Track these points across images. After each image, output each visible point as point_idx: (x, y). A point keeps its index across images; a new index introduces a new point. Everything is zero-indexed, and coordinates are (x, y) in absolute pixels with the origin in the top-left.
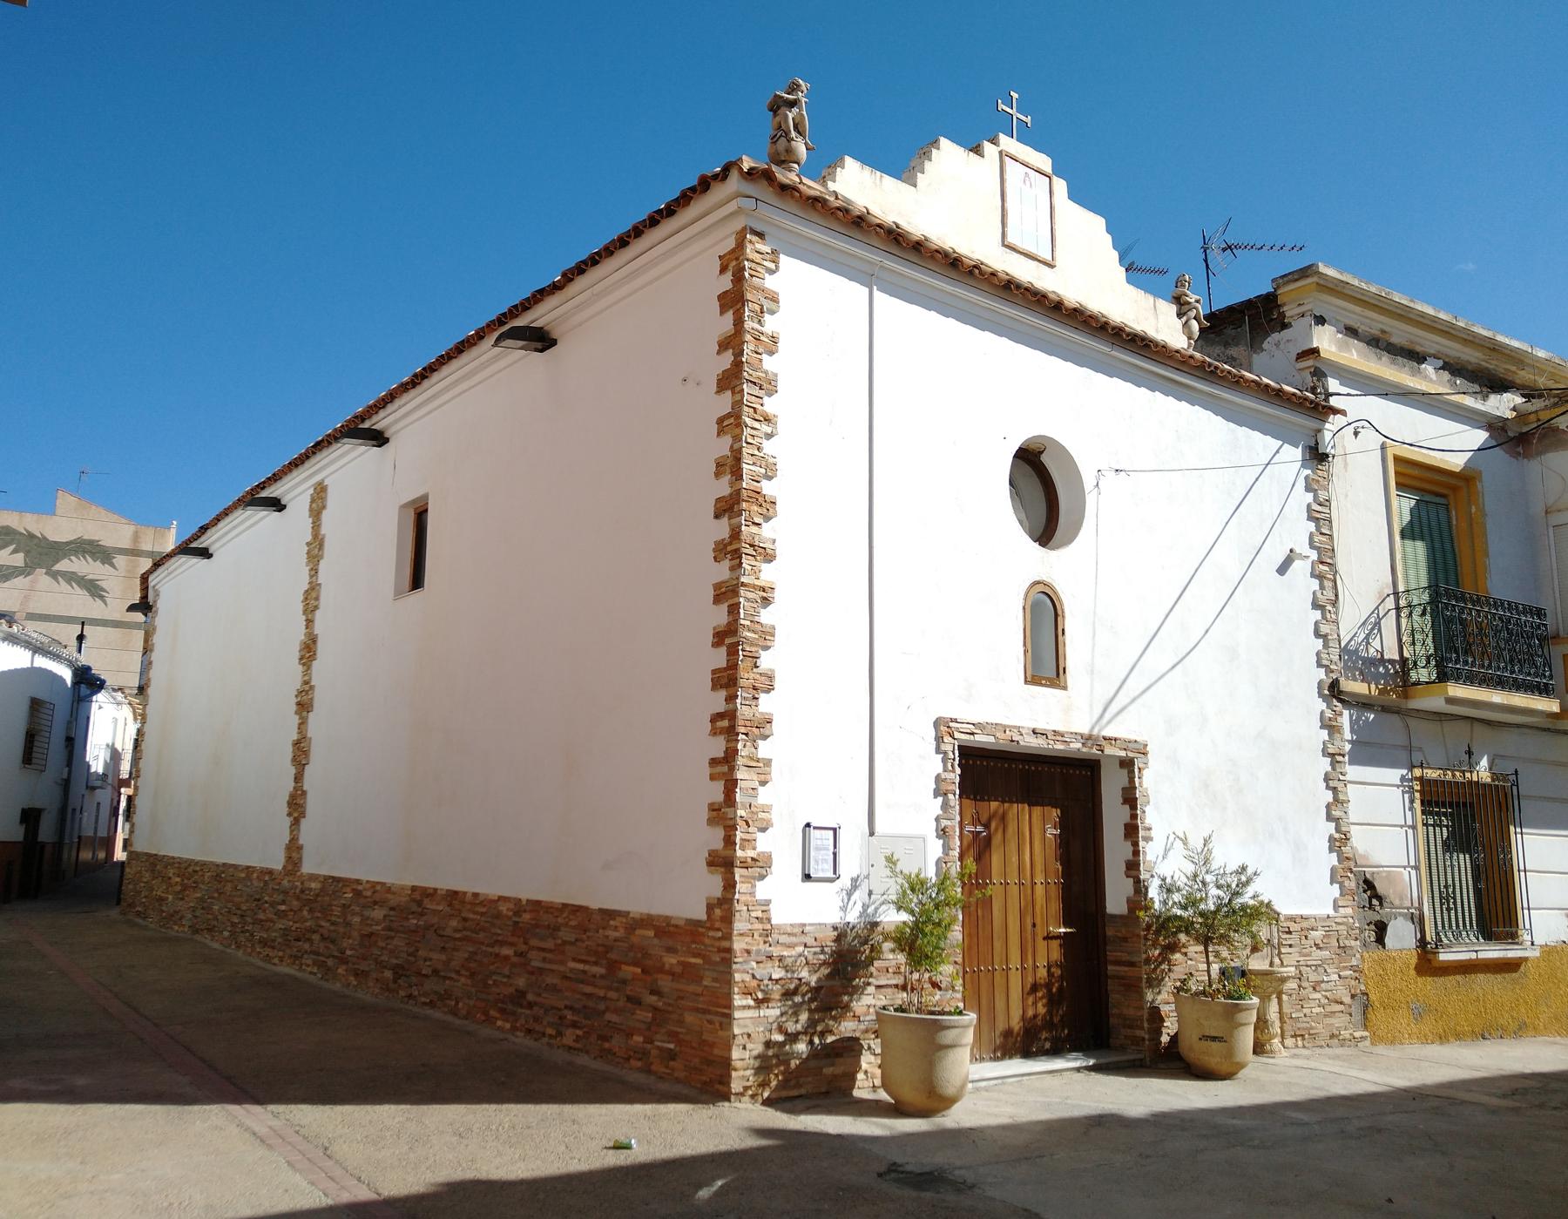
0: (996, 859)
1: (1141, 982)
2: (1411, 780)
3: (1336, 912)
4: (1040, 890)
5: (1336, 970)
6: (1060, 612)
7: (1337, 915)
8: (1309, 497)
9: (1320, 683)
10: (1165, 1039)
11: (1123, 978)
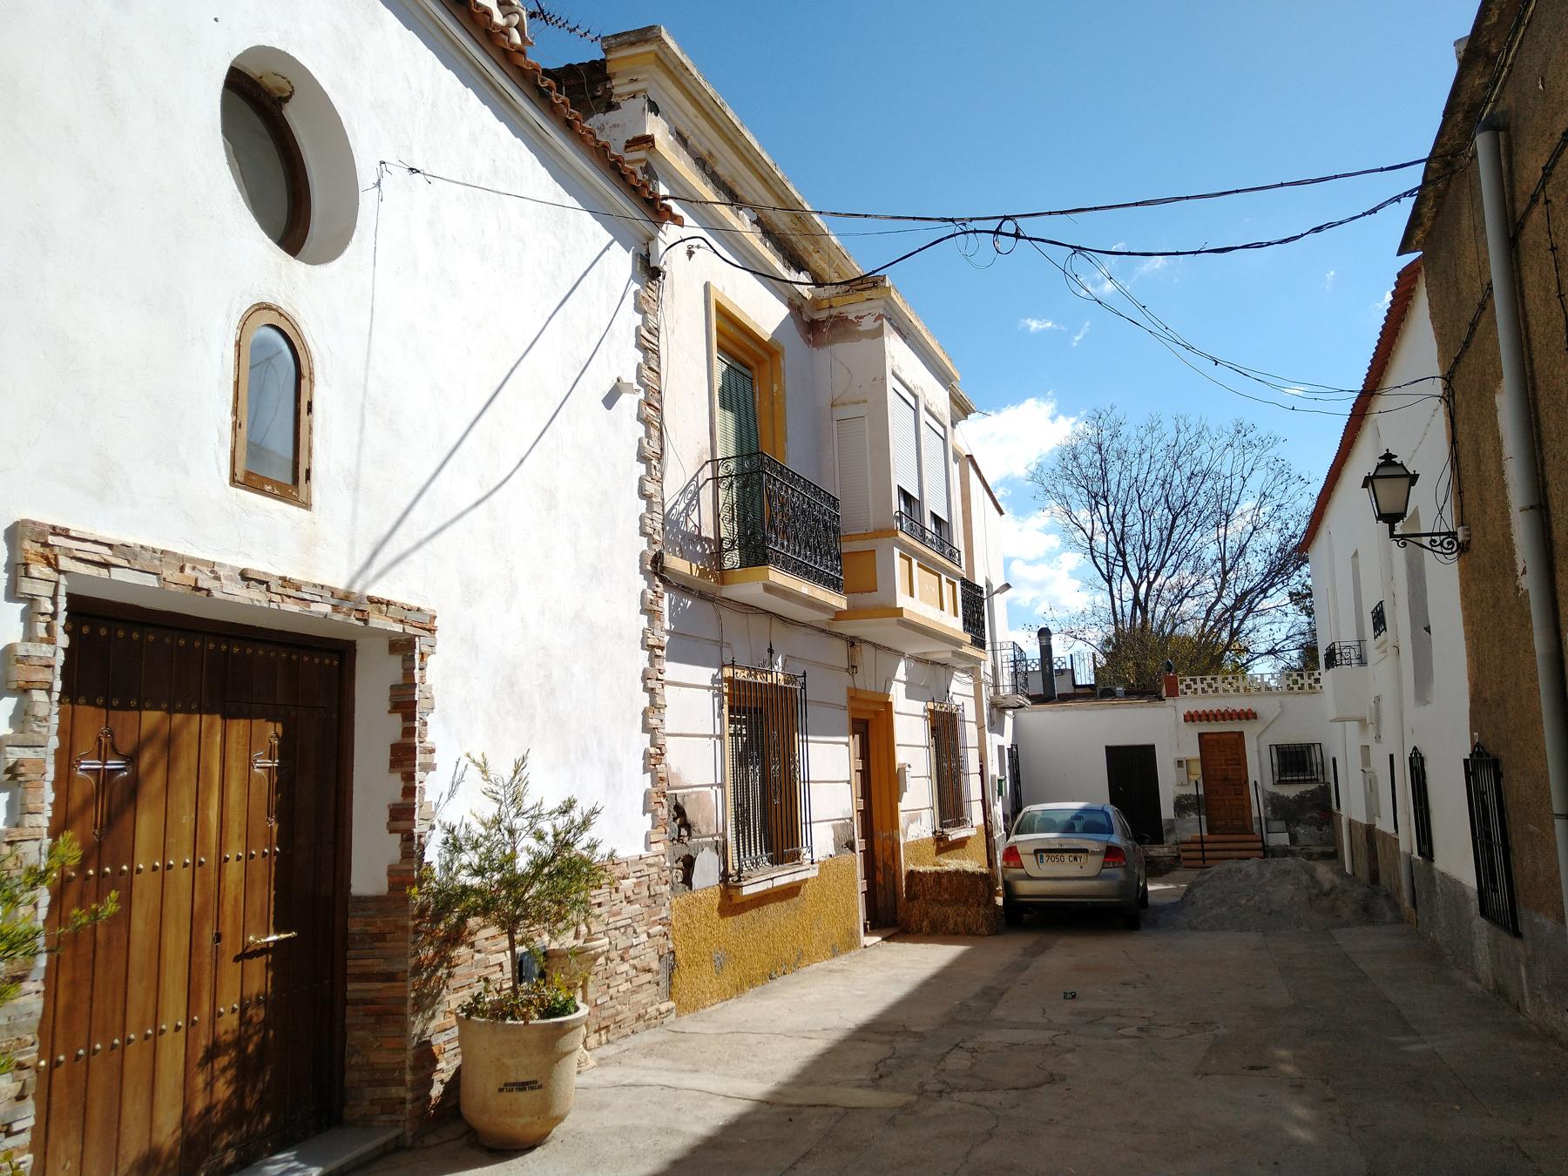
0: (146, 824)
1: (405, 1005)
2: (721, 681)
3: (647, 850)
4: (234, 871)
5: (646, 928)
6: (305, 371)
7: (650, 854)
8: (638, 319)
9: (643, 555)
10: (436, 1091)
11: (373, 1002)
